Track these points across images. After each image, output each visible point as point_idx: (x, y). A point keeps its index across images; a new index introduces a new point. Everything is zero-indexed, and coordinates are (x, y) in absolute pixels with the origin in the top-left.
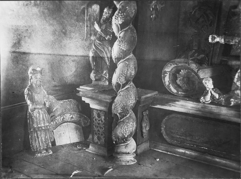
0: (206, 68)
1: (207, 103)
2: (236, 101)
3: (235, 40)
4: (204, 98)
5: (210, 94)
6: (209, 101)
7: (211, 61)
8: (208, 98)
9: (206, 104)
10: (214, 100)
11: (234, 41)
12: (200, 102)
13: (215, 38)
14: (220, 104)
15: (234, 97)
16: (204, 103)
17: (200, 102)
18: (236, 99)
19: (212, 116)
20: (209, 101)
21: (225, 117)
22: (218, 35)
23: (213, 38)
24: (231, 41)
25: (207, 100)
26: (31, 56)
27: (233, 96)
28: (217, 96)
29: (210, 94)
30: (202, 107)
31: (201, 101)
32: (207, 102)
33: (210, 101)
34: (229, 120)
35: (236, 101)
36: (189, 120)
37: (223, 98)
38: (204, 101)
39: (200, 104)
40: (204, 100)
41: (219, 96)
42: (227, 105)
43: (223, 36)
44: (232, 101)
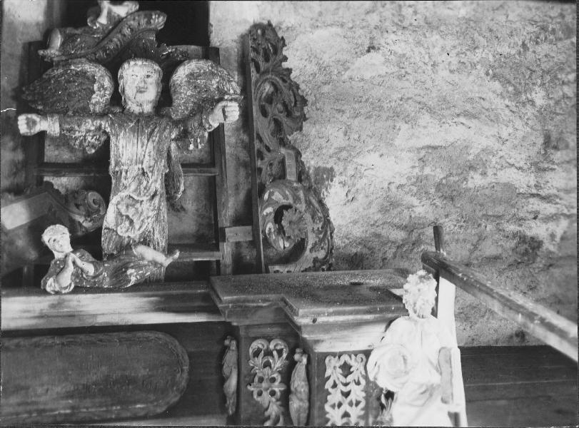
0: (12, 202)
1: (67, 291)
2: (141, 272)
3: (30, 132)
4: (56, 281)
5: (71, 269)
6: (70, 285)
7: (299, 163)
8: (67, 279)
9: (65, 294)
10: (82, 279)
11: (83, 128)
12: (45, 293)
13: (34, 123)
14: (98, 288)
15: (132, 264)
16: (57, 293)
17: (45, 293)
18: (139, 267)
19: (76, 323)
20: (70, 285)
21: (123, 316)
22: (43, 114)
23: (31, 124)
24: (76, 128)
25: (65, 285)
26: (434, 282)
27: (129, 263)
28: (90, 269)
29: (71, 269)
30: (53, 306)
31: (48, 289)
32: (66, 288)
33: (73, 286)
34: (120, 323)
35: (141, 272)
36: (13, 347)
37: (106, 269)
38: (57, 289)
39: (48, 298)
40: (56, 285)
41: (96, 270)
42: (119, 284)
43: (56, 117)
44: (131, 275)
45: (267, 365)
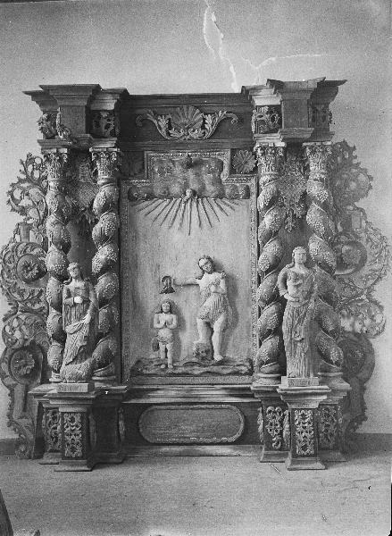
45: (274, 417)
